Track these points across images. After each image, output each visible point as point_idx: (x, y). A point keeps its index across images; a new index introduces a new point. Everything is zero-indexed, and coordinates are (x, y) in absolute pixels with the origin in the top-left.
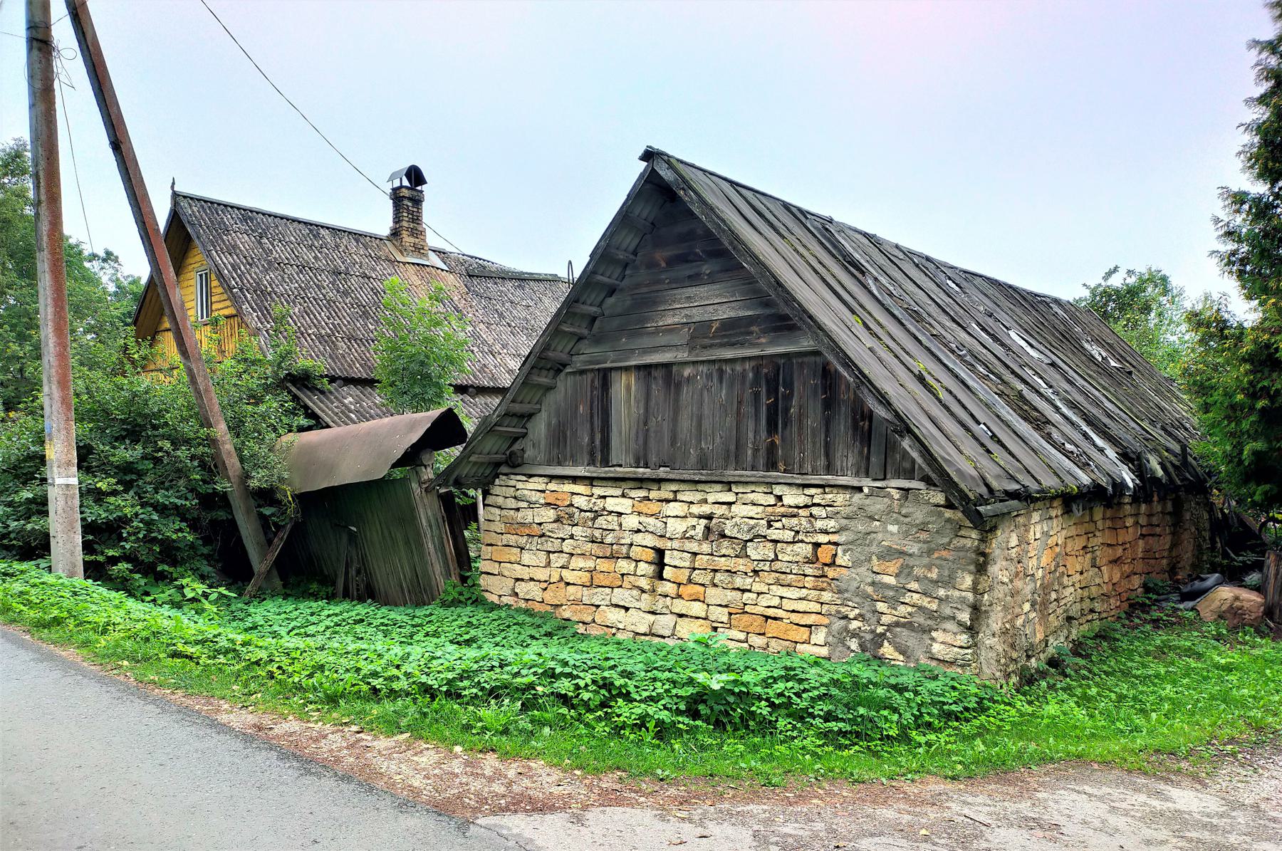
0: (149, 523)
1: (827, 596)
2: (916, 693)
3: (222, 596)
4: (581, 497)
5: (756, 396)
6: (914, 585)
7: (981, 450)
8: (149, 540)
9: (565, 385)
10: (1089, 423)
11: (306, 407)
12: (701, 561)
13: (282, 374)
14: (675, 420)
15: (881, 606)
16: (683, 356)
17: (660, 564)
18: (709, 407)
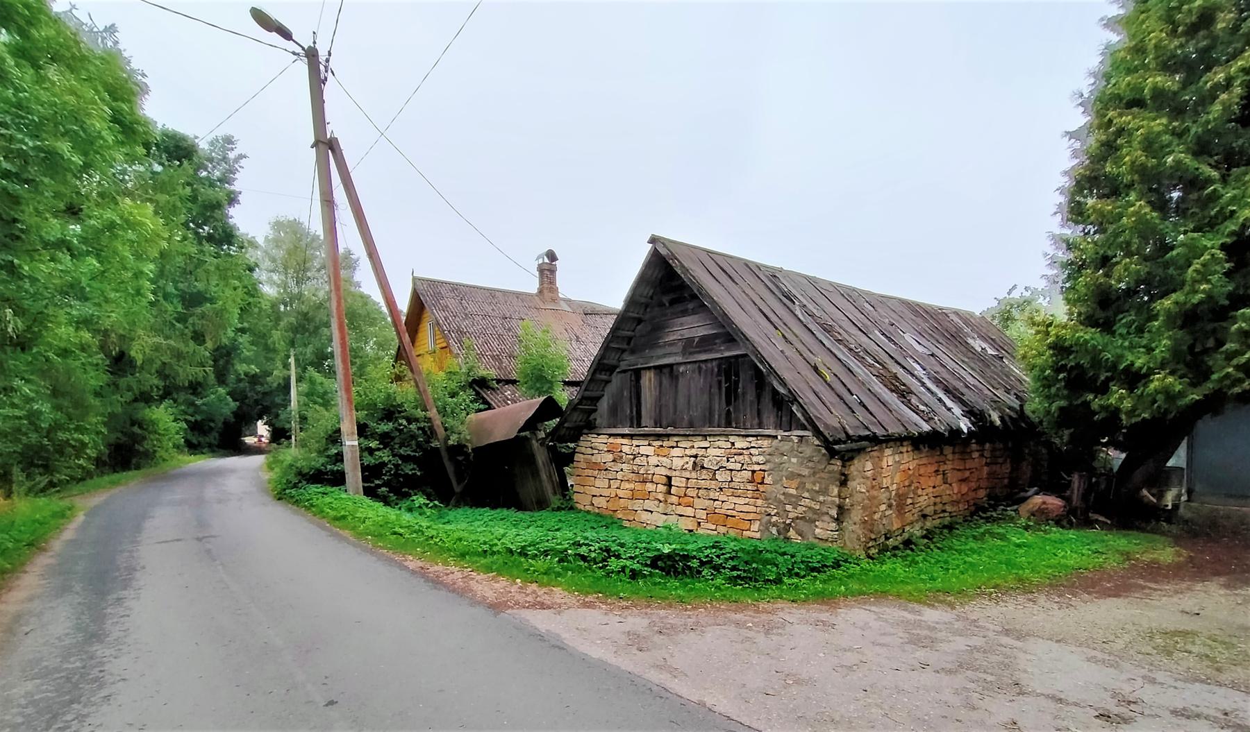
0: (397, 466)
1: (759, 502)
2: (793, 556)
3: (435, 506)
4: (627, 446)
5: (720, 382)
6: (806, 495)
7: (848, 411)
8: (396, 475)
9: (616, 380)
10: (947, 391)
11: (483, 398)
12: (692, 483)
13: (470, 379)
14: (676, 399)
15: (788, 507)
16: (679, 359)
17: (669, 485)
18: (695, 389)
